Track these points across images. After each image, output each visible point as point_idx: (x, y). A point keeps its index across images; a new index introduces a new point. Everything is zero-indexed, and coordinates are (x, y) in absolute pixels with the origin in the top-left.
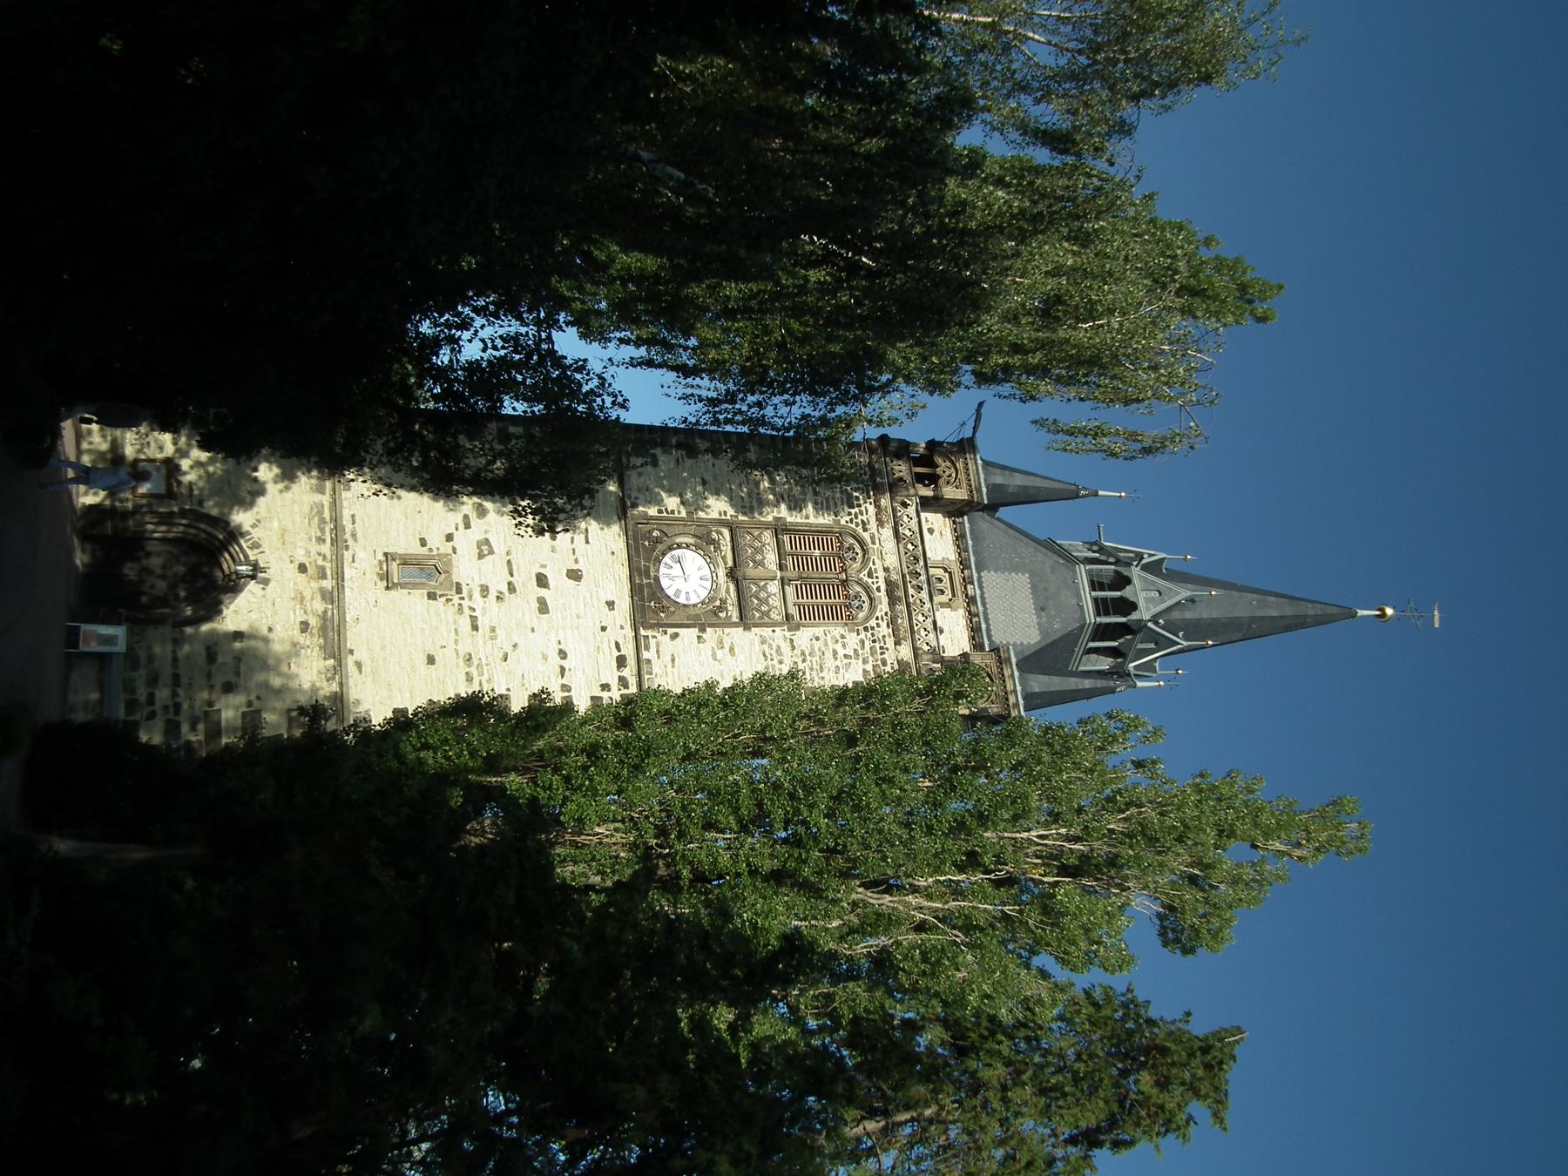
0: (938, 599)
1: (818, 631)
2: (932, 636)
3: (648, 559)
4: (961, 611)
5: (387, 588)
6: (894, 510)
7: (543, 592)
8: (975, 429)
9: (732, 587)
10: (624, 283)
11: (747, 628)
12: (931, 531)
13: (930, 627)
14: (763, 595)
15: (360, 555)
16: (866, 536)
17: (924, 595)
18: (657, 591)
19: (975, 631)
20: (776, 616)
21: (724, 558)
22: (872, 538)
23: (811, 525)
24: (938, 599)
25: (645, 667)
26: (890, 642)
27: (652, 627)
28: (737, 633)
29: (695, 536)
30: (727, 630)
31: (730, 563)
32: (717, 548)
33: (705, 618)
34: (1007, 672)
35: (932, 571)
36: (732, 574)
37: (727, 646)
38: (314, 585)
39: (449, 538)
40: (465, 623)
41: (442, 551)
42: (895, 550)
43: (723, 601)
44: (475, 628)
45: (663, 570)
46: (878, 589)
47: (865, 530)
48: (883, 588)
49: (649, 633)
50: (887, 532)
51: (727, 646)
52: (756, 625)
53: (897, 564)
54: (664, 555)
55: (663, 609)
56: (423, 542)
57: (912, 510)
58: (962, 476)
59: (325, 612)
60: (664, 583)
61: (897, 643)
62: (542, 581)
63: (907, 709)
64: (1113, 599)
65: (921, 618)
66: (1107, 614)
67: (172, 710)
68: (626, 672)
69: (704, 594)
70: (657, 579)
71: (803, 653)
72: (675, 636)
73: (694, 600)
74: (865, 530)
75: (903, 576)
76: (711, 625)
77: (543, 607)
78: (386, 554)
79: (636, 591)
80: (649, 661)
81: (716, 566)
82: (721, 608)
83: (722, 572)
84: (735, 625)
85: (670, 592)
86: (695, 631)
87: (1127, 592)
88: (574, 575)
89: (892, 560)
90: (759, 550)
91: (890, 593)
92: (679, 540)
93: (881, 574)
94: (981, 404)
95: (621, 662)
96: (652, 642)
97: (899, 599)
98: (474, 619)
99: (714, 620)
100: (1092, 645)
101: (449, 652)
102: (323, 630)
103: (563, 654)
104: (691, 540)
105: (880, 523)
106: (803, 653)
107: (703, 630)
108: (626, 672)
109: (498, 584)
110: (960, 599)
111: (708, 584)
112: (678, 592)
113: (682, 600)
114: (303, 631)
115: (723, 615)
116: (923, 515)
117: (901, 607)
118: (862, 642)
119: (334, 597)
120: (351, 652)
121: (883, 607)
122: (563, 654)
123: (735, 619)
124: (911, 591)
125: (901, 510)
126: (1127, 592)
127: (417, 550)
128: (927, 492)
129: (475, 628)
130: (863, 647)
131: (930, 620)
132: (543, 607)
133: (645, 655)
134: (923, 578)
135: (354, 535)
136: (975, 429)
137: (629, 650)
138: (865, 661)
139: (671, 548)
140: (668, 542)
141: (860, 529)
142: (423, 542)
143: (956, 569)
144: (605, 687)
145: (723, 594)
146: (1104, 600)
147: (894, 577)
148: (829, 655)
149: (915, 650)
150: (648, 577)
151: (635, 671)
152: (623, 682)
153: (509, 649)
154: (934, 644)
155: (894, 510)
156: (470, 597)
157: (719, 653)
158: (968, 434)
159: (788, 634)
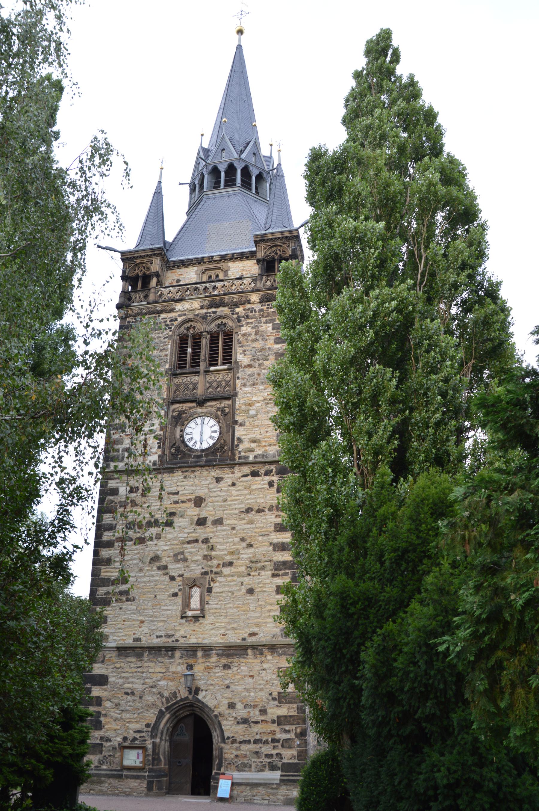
0: (221, 277)
1: (240, 350)
2: (245, 281)
3: (190, 456)
4: (230, 264)
5: (203, 617)
6: (164, 302)
7: (209, 522)
8: (115, 251)
9: (209, 404)
10: (455, 237)
11: (236, 395)
12: (178, 281)
13: (240, 282)
14: (215, 384)
15: (182, 633)
16: (180, 319)
17: (218, 284)
18: (211, 451)
19: (242, 256)
20: (229, 377)
21: (190, 408)
22: (180, 316)
23: (171, 353)
24: (221, 277)
25: (259, 459)
26: (248, 306)
27: (233, 454)
28: (239, 402)
29: (176, 426)
30: (237, 407)
31: (194, 404)
32: (184, 412)
33: (228, 421)
34: (270, 237)
35: (204, 280)
36: (201, 403)
37: (247, 408)
38: (200, 660)
39: (172, 578)
40: (226, 571)
41: (180, 583)
42: (190, 302)
43: (218, 409)
44: (231, 564)
45: (197, 447)
46: (214, 313)
47: (176, 320)
48: (213, 310)
49: (237, 458)
50: (179, 306)
51: (247, 408)
52: (234, 389)
53: (198, 301)
54: (187, 446)
55: (222, 447)
56: (175, 595)
57: (165, 291)
58: (144, 260)
59: (218, 655)
60: (205, 446)
61: (249, 302)
62: (201, 522)
63: (420, 176)
64: (226, 176)
65: (234, 287)
66: (234, 180)
67: (276, 744)
68: (262, 471)
69: (213, 422)
70: (203, 451)
71: (254, 360)
72: (239, 440)
73: (217, 428)
74: (176, 320)
75: (206, 297)
76: (233, 417)
77: (219, 522)
78: (182, 617)
79: (209, 465)
80: (255, 457)
81: (196, 413)
82: (223, 410)
83: (200, 410)
85: (211, 442)
86: (237, 427)
87: (222, 168)
88: (199, 502)
89: (196, 304)
90: (186, 387)
91: (217, 306)
92: (178, 436)
93: (205, 311)
94: (99, 247)
95: (255, 474)
96: (243, 454)
97: (221, 300)
98: (224, 565)
99: (230, 415)
100: (254, 190)
101: (246, 580)
102: (228, 656)
103: (248, 510)
104: (178, 429)
105: (172, 310)
107: (236, 422)
108: (262, 471)
109: (203, 549)
110: (223, 265)
111: (207, 419)
112: (211, 437)
113: (216, 435)
114: (229, 668)
115: (227, 410)
116: (167, 284)
117: (227, 298)
118: (247, 323)
119: (207, 650)
120: (244, 639)
121: (225, 310)
122: (248, 510)
123: (229, 402)
124: (216, 292)
125: (165, 297)
126: (222, 168)
127: (179, 600)
128: (154, 282)
129: (231, 564)
130: (251, 323)
131: (235, 282)
132: (219, 522)
133: (251, 458)
134: (208, 285)
135: (169, 636)
136: (115, 251)
137: (246, 469)
138: (260, 322)
139: (183, 442)
140: (179, 443)
141: (176, 323)
142: (175, 595)
143: (203, 267)
144: (271, 484)
145: (213, 410)
146: (226, 181)
147: (206, 303)
148: (255, 345)
149: (254, 291)
150: (200, 456)
151: (260, 465)
152: (267, 473)
153: (244, 544)
154: (250, 280)
155: (164, 302)
156: (211, 566)
157: (252, 412)
158: (119, 255)
159: (241, 370)
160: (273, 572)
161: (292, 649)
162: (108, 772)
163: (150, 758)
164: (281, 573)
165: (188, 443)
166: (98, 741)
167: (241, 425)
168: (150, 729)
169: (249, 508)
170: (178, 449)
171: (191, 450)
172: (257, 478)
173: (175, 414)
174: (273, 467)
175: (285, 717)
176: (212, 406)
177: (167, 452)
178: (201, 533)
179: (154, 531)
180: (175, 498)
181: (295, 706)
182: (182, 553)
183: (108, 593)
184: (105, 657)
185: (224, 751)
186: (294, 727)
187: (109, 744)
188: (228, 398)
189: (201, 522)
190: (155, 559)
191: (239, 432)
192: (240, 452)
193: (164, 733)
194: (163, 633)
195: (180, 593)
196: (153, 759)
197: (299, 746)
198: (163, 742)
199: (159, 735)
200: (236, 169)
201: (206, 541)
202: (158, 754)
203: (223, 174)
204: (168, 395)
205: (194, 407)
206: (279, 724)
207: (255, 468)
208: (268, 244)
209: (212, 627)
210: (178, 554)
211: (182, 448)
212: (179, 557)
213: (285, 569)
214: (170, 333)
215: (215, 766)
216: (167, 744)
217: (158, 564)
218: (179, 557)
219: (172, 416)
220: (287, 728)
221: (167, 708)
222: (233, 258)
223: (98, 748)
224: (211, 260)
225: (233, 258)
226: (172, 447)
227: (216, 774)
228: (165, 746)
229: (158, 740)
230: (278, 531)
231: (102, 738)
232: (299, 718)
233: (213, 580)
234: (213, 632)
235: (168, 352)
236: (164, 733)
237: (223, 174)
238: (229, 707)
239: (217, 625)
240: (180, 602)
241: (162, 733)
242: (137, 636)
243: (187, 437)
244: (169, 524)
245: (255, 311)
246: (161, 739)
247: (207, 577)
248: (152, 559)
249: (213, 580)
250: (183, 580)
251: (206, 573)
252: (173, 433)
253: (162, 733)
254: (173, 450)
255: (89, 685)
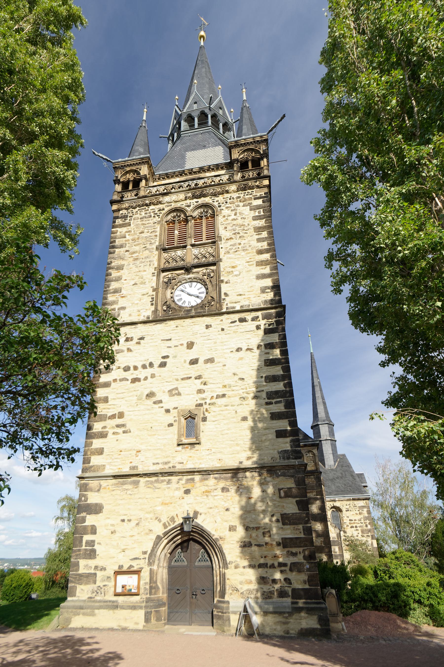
9: (195, 270)
15: (178, 459)
16: (167, 209)
26: (226, 195)
27: (221, 306)
29: (166, 288)
31: (183, 271)
33: (213, 283)
36: (188, 270)
37: (231, 270)
38: (198, 484)
39: (168, 411)
47: (163, 209)
50: (167, 199)
51: (231, 270)
52: (219, 256)
62: (194, 362)
71: (235, 234)
72: (226, 294)
77: (210, 361)
78: (179, 445)
80: (241, 307)
84: (219, 268)
86: (223, 286)
87: (196, 115)
88: (190, 345)
89: (182, 196)
95: (242, 320)
96: (229, 305)
98: (218, 397)
106: (235, 234)
111: (194, 284)
118: (227, 207)
126: (196, 115)
130: (231, 207)
135: (166, 463)
138: (238, 206)
141: (163, 212)
142: (171, 425)
144: (258, 327)
153: (236, 378)
160: (267, 400)
161: (292, 471)
162: (102, 604)
163: (148, 587)
164: (274, 401)
165: (178, 303)
166: (92, 571)
167: (226, 283)
168: (147, 556)
169: (238, 348)
170: (169, 307)
171: (180, 307)
172: (244, 323)
173: (166, 280)
174: (259, 314)
175: (291, 539)
176: (198, 273)
177: (159, 308)
178: (194, 371)
179: (149, 371)
180: (169, 343)
181: (301, 527)
182: (176, 389)
183: (105, 427)
184: (101, 486)
185: (227, 576)
186: (301, 549)
187: (103, 573)
188: (214, 264)
189: (194, 362)
190: (151, 395)
191: (224, 288)
192: (227, 304)
193: (162, 560)
194: (160, 461)
195: (174, 424)
196: (151, 588)
197: (308, 570)
198: (160, 569)
199: (156, 562)
200: (207, 116)
201: (199, 377)
202: (156, 582)
203: (196, 120)
204: (159, 265)
205: (182, 274)
206: (284, 547)
207: (242, 315)
208: (241, 148)
209: (208, 452)
210: (173, 389)
211: (173, 305)
212: (174, 392)
213: (278, 398)
214: (159, 219)
215: (217, 594)
216: (165, 571)
217: (154, 399)
218: (174, 392)
219: (163, 281)
220: (294, 550)
221: (165, 534)
222: (210, 169)
223: (90, 578)
224: (191, 172)
225: (210, 169)
226: (164, 305)
227: (219, 602)
228: (162, 574)
229: (155, 567)
230: (268, 366)
231: (96, 568)
232: (305, 540)
233: (207, 410)
234: (210, 457)
235: (158, 234)
236: (162, 560)
237: (196, 120)
238: (230, 530)
239: (213, 450)
240: (176, 432)
241: (159, 559)
242: (133, 464)
243: (176, 299)
244: (163, 365)
245: (233, 198)
246: (158, 566)
247: (202, 408)
248: (147, 395)
249: (207, 410)
250: (178, 412)
251: (201, 405)
252: (164, 294)
253: (159, 559)
254: (165, 308)
255: (84, 514)
